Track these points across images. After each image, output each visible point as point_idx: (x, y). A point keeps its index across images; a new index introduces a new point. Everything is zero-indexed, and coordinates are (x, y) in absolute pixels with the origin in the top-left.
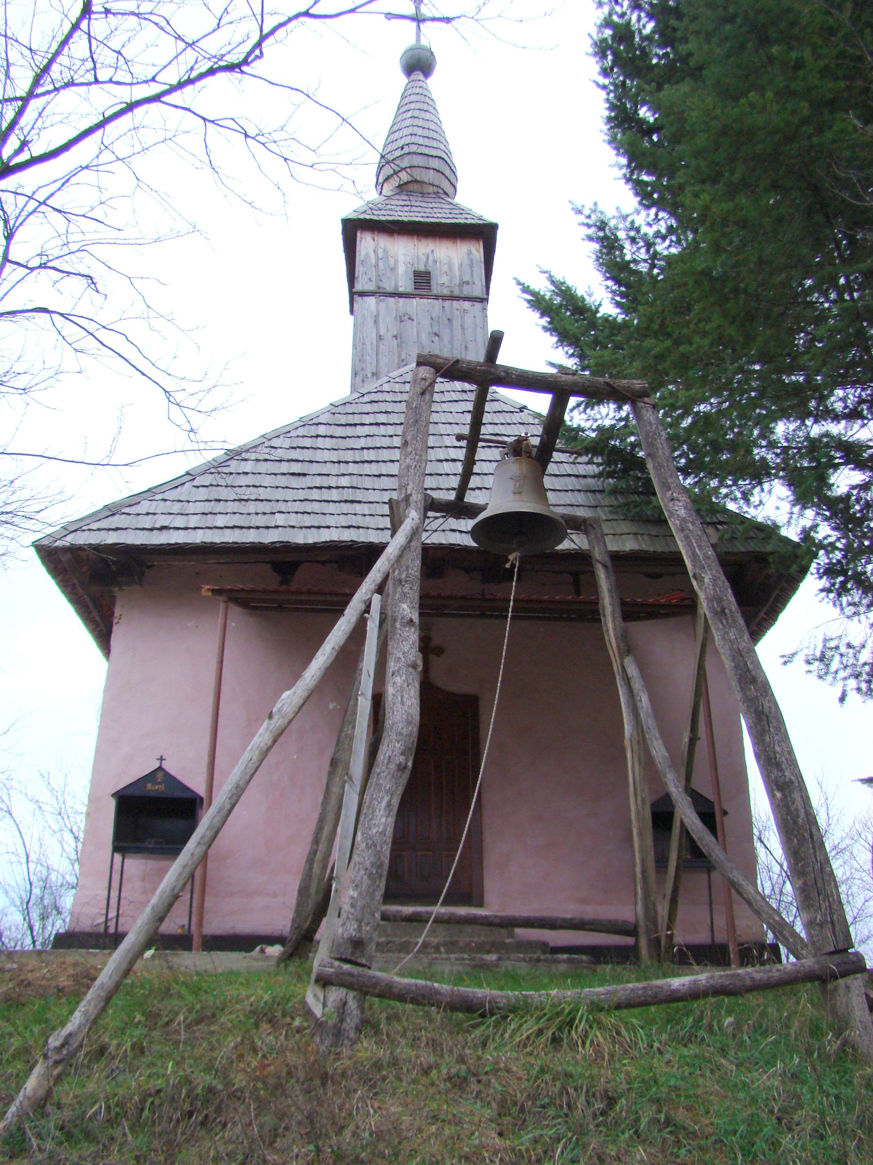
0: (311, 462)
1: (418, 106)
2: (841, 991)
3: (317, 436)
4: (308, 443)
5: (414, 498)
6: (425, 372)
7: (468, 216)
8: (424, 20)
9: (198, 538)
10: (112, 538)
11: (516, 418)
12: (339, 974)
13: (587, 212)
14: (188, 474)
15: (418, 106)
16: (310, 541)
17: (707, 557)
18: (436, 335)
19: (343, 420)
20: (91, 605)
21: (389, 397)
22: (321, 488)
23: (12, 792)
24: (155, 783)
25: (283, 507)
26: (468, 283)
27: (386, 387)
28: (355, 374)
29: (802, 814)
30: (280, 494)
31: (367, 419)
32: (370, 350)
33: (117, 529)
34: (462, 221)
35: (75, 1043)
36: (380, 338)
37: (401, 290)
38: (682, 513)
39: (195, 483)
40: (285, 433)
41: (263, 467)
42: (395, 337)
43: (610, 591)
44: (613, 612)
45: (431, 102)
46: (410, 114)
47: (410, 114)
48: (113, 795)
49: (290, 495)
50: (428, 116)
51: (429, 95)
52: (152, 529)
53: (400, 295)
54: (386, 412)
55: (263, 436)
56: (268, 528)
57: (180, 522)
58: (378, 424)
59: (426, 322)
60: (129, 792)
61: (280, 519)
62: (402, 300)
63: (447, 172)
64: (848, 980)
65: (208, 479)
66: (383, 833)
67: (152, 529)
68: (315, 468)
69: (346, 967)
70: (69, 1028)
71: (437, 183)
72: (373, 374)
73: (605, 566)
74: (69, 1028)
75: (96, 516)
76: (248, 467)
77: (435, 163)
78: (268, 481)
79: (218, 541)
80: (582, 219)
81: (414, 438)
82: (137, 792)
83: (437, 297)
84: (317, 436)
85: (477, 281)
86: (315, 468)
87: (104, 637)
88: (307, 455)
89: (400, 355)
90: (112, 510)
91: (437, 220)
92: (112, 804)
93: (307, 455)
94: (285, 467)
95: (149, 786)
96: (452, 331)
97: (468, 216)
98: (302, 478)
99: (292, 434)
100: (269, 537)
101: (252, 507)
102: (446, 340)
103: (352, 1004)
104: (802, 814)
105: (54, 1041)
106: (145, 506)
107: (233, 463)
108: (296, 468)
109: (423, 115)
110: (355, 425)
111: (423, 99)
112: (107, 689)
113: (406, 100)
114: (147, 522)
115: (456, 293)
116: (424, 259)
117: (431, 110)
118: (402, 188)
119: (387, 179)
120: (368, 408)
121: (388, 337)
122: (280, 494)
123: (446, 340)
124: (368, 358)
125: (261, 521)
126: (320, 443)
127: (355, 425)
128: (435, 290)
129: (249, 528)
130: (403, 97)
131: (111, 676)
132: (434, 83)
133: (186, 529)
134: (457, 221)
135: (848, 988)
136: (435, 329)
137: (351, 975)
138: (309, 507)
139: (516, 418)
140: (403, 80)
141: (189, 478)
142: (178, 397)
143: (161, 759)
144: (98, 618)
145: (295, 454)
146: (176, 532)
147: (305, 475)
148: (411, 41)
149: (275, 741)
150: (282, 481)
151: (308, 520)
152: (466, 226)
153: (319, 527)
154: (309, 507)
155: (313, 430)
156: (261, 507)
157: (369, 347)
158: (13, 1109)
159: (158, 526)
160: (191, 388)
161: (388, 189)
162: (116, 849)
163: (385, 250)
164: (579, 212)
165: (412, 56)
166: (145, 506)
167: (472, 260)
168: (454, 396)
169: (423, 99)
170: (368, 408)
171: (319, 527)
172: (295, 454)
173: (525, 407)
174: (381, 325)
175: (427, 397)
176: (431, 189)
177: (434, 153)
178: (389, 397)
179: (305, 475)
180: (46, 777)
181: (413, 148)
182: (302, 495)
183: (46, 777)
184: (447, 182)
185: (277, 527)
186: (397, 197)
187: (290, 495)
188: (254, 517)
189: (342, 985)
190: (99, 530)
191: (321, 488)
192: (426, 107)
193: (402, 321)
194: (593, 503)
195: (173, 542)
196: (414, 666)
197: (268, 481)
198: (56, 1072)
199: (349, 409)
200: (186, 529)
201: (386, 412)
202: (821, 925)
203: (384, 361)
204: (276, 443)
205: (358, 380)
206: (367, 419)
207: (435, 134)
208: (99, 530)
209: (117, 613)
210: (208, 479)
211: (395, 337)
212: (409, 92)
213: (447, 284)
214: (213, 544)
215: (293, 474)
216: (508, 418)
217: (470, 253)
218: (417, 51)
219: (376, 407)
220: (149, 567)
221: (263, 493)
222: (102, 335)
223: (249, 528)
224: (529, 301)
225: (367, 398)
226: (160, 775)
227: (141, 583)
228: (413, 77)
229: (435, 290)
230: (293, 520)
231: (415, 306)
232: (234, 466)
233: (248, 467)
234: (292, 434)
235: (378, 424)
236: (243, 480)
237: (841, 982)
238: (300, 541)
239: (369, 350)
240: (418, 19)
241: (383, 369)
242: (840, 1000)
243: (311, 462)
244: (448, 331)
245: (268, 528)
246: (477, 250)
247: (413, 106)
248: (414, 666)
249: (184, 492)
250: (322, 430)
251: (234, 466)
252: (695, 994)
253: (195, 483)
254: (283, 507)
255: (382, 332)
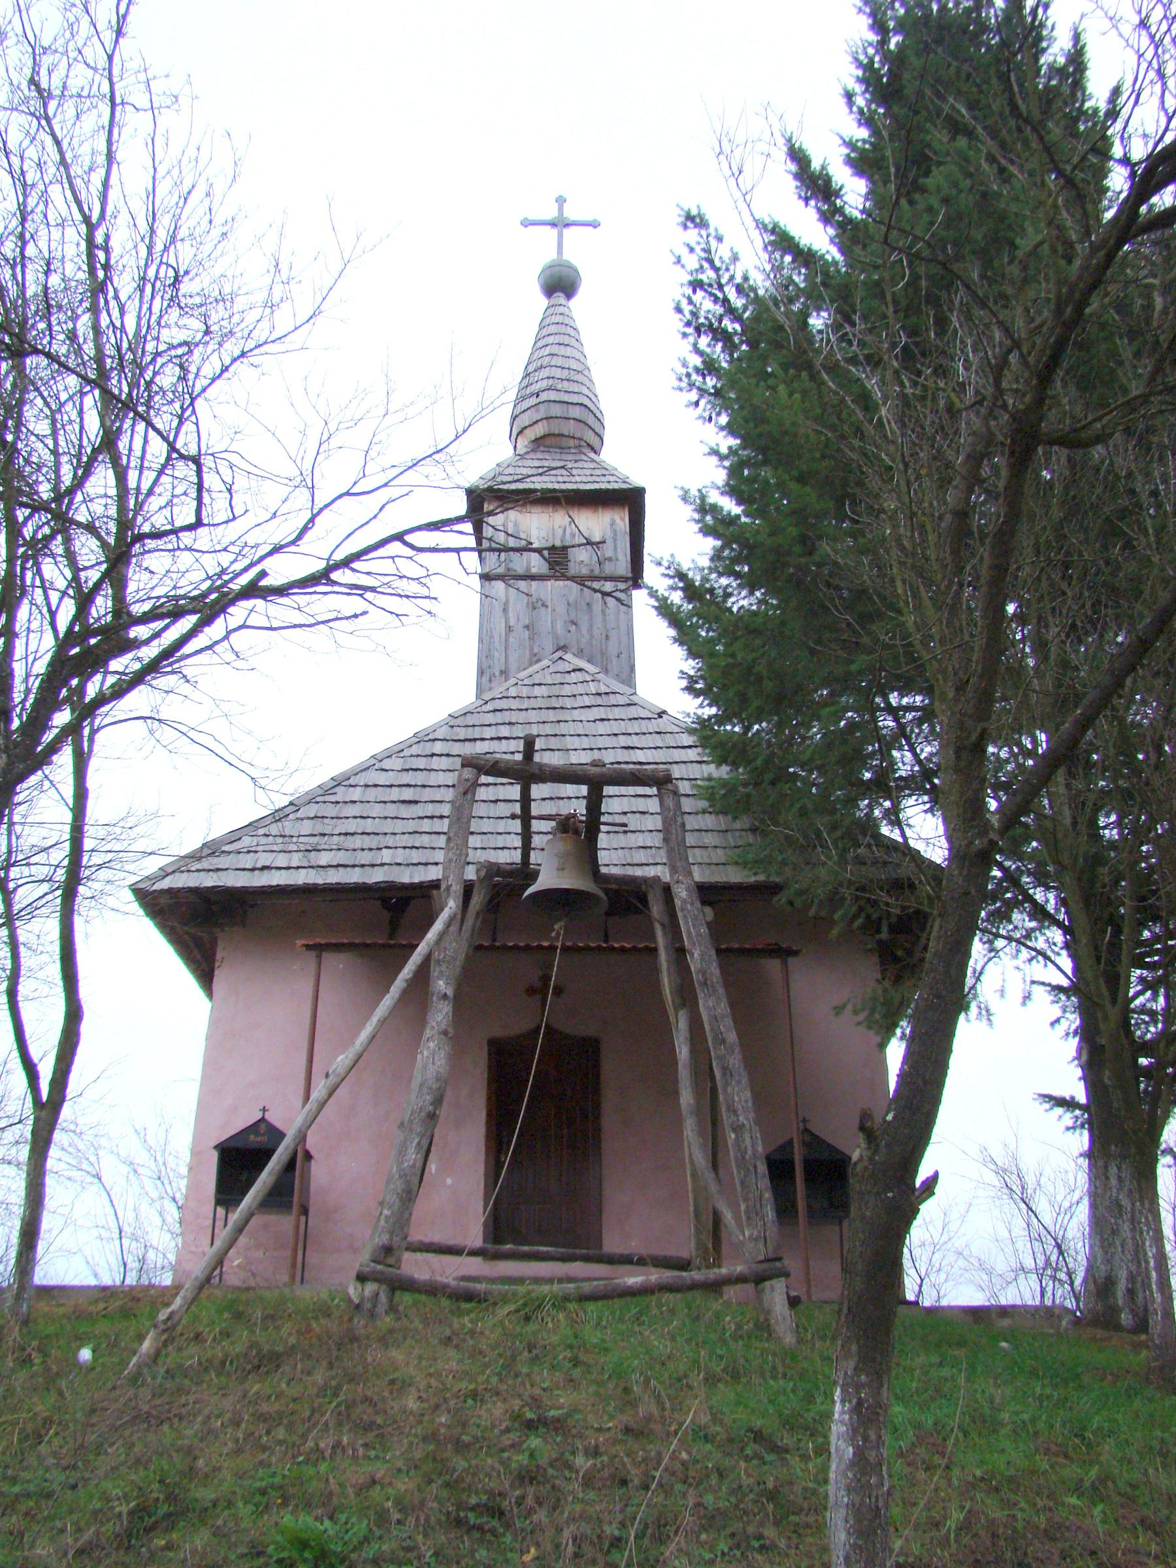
0: (424, 786)
1: (557, 339)
2: (767, 1291)
3: (433, 755)
4: (421, 763)
5: (454, 888)
6: (468, 773)
7: (612, 479)
8: (567, 225)
9: (301, 878)
10: (209, 881)
11: (652, 726)
12: (373, 1272)
13: (666, 564)
14: (291, 804)
15: (557, 339)
16: (416, 880)
17: (699, 935)
18: (573, 623)
19: (462, 733)
20: (192, 945)
21: (514, 704)
22: (432, 817)
23: (101, 1153)
24: (257, 1134)
25: (390, 841)
26: (610, 559)
27: (513, 692)
28: (481, 672)
29: (750, 1152)
30: (388, 826)
31: (488, 733)
32: (498, 644)
33: (218, 870)
34: (603, 486)
35: (176, 1318)
36: (509, 629)
37: (534, 571)
38: (684, 894)
39: (299, 815)
40: (397, 752)
41: (372, 794)
42: (527, 627)
43: (666, 948)
44: (669, 969)
45: (572, 333)
46: (547, 351)
47: (547, 351)
48: (216, 1147)
49: (399, 826)
50: (568, 352)
51: (571, 323)
52: (253, 870)
53: (533, 578)
54: (510, 723)
55: (373, 757)
56: (373, 866)
57: (282, 861)
58: (499, 739)
59: (561, 609)
60: (233, 1144)
61: (386, 856)
62: (534, 583)
63: (591, 421)
64: (774, 1282)
65: (312, 810)
66: (413, 1166)
67: (253, 870)
68: (428, 794)
69: (379, 1267)
70: (173, 1307)
71: (578, 435)
72: (502, 672)
73: (663, 925)
74: (173, 1307)
75: (195, 856)
76: (356, 794)
77: (575, 412)
78: (377, 810)
79: (320, 881)
80: (662, 570)
81: (456, 834)
82: (239, 1144)
83: (572, 579)
84: (433, 755)
85: (621, 557)
86: (428, 794)
87: (206, 977)
88: (419, 778)
89: (531, 649)
90: (212, 849)
91: (574, 487)
92: (214, 1156)
93: (419, 778)
94: (395, 794)
95: (252, 1137)
96: (591, 618)
97: (612, 479)
98: (414, 807)
99: (405, 753)
100: (376, 876)
101: (357, 842)
102: (584, 630)
103: (383, 1298)
104: (750, 1152)
105: (162, 1316)
106: (247, 841)
107: (340, 790)
108: (408, 794)
109: (563, 351)
110: (475, 740)
111: (563, 329)
112: (209, 1037)
113: (544, 332)
114: (248, 861)
115: (597, 572)
116: (560, 532)
117: (573, 342)
118: (539, 443)
119: (520, 433)
120: (490, 718)
121: (518, 628)
122: (388, 826)
123: (584, 630)
124: (496, 654)
125: (366, 858)
126: (436, 763)
127: (475, 740)
128: (573, 569)
129: (354, 866)
130: (535, 349)
131: (215, 1022)
132: (578, 306)
133: (288, 868)
134: (597, 486)
135: (772, 1288)
136: (573, 616)
137: (382, 1273)
138: (418, 841)
139: (652, 726)
140: (543, 302)
141: (293, 809)
142: (263, 782)
143: (264, 1110)
144: (199, 957)
145: (407, 778)
146: (278, 873)
147: (416, 802)
148: (550, 256)
149: (330, 1095)
150: (391, 810)
151: (416, 856)
152: (607, 492)
153: (426, 864)
154: (418, 841)
155: (428, 748)
156: (368, 841)
157: (497, 640)
158: (134, 1360)
159: (259, 865)
160: (273, 775)
161: (522, 444)
162: (219, 1202)
163: (516, 525)
164: (659, 564)
165: (552, 276)
166: (247, 841)
167: (615, 532)
168: (587, 701)
169: (563, 329)
170: (490, 718)
171: (426, 864)
172: (407, 778)
173: (664, 712)
174: (511, 614)
175: (469, 796)
176: (572, 443)
177: (575, 399)
178: (514, 704)
179: (416, 802)
180: (141, 1134)
181: (553, 396)
182: (411, 826)
183: (141, 1134)
184: (591, 432)
185: (382, 865)
186: (532, 455)
187: (399, 826)
188: (359, 853)
189: (376, 1280)
190: (198, 871)
191: (432, 817)
192: (566, 340)
193: (534, 608)
194: (724, 828)
195: (274, 883)
196: (445, 1033)
197: (377, 810)
198: (164, 1337)
199: (470, 720)
200: (288, 868)
201: (510, 723)
202: (756, 1240)
203: (514, 656)
204: (387, 764)
205: (485, 679)
206: (488, 733)
207: (578, 374)
208: (198, 871)
209: (219, 956)
210: (312, 810)
211: (527, 627)
212: (547, 321)
213: (587, 561)
214: (315, 886)
215: (404, 802)
216: (645, 726)
217: (613, 524)
218: (556, 269)
219: (499, 717)
220: (252, 906)
221: (369, 825)
222: (192, 734)
223: (354, 866)
224: (656, 608)
225: (489, 707)
226: (263, 1126)
227: (244, 925)
228: (554, 301)
229: (573, 569)
230: (401, 856)
231: (552, 589)
232: (341, 794)
233: (356, 794)
234: (405, 753)
235: (499, 739)
236: (351, 810)
237: (767, 1284)
238: (406, 879)
239: (497, 644)
240: (560, 224)
241: (513, 666)
242: (766, 1296)
243: (424, 786)
244: (586, 617)
245: (373, 866)
246: (620, 519)
247: (551, 340)
248: (445, 1033)
249: (288, 827)
250: (438, 747)
251: (341, 794)
252: (645, 1291)
253: (299, 815)
254: (390, 841)
255: (512, 623)
